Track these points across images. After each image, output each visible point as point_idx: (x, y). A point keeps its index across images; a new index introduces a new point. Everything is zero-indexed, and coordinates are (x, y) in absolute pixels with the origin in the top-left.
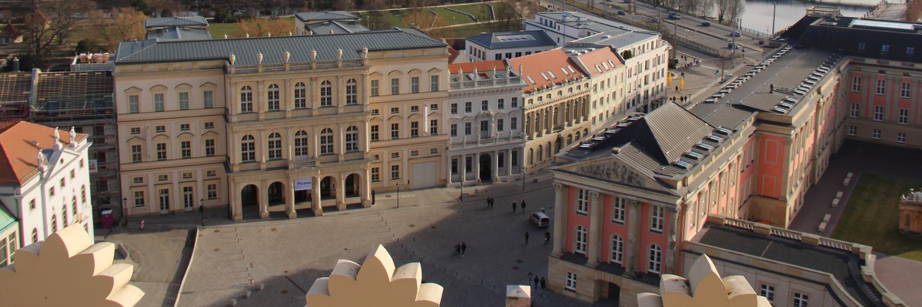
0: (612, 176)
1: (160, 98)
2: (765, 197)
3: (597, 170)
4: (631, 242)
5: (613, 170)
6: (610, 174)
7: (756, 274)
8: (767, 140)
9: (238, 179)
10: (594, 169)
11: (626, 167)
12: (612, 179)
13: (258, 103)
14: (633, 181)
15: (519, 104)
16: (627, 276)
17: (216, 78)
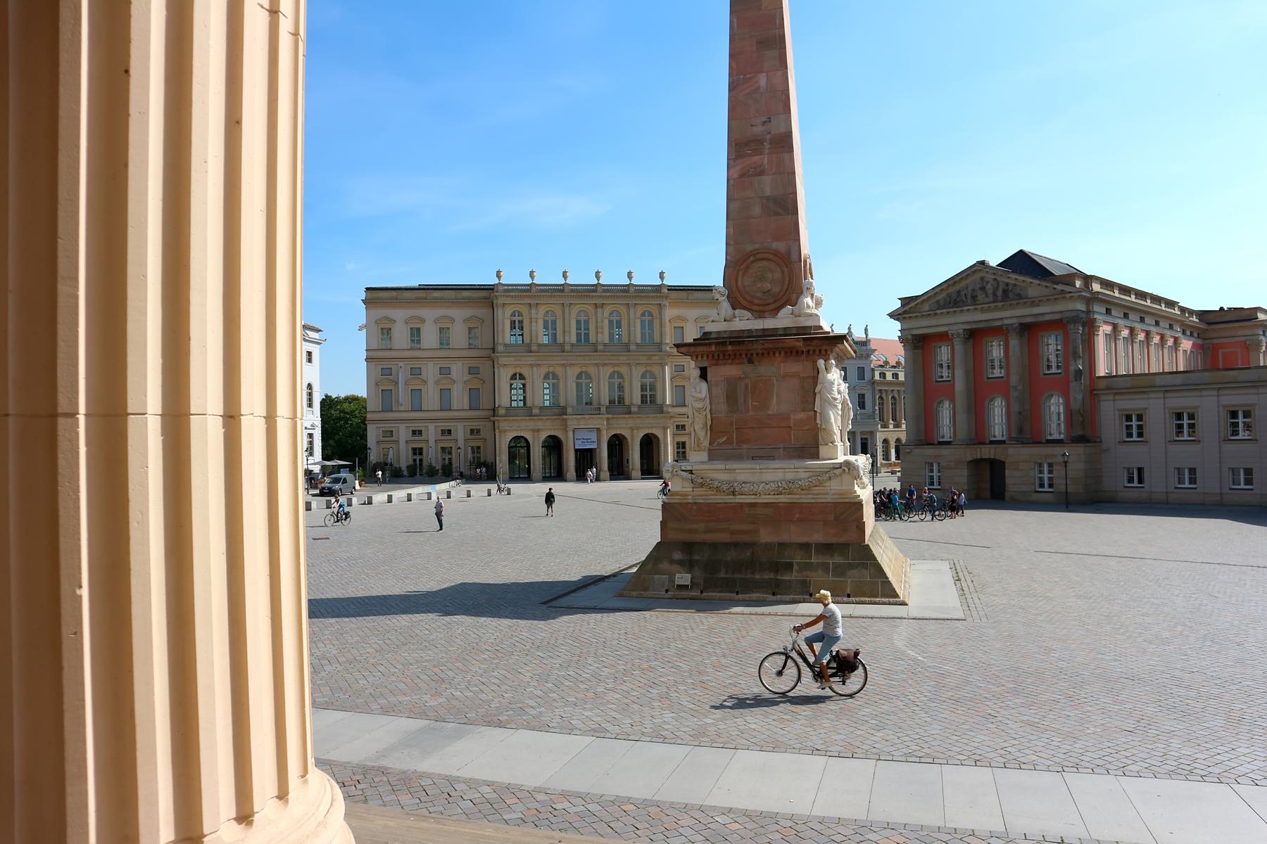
1: (416, 334)
4: (1015, 388)
6: (977, 296)
7: (1218, 396)
8: (1221, 352)
9: (503, 425)
13: (531, 331)
15: (867, 376)
17: (482, 312)
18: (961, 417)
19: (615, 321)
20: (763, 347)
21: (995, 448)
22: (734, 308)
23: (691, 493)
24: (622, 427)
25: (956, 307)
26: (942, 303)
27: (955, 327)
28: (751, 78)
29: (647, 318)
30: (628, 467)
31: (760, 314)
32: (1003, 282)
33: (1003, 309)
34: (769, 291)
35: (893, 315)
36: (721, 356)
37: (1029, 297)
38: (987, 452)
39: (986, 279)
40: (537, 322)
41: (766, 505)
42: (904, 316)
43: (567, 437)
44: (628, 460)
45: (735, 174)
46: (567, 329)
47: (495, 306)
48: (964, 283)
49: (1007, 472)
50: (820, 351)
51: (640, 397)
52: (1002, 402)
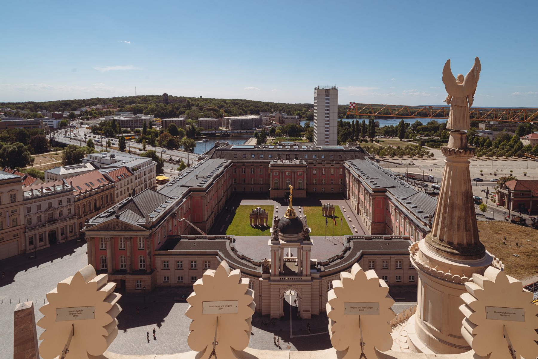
2: (197, 223)
5: (116, 225)
8: (195, 199)
10: (107, 226)
11: (123, 222)
12: (117, 229)
14: (127, 228)
35: (14, 281)
49: (126, 284)
51: (514, 225)
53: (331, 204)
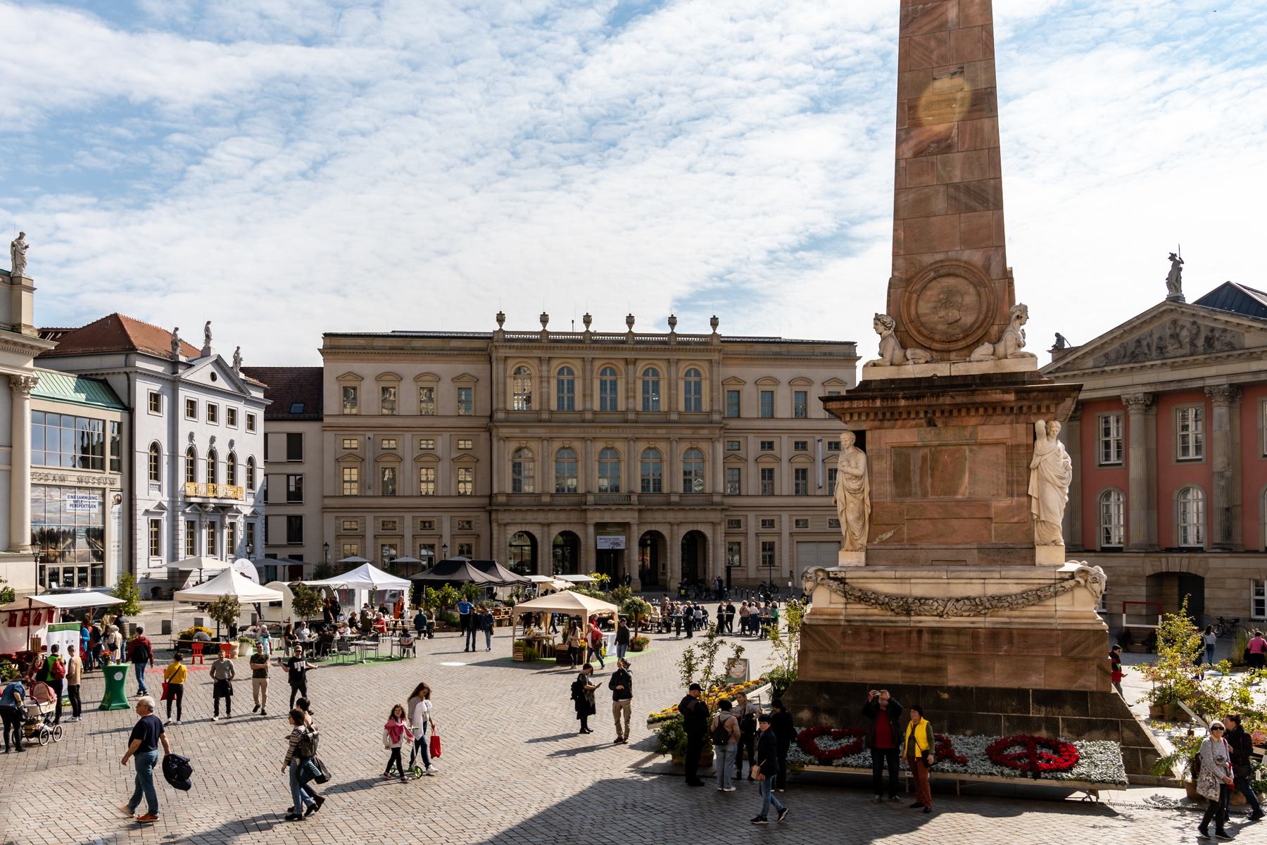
0: (1170, 348)
3: (1137, 347)
5: (1172, 336)
6: (1166, 347)
16: (1219, 550)
18: (1137, 513)
19: (651, 383)
20: (954, 401)
21: (1189, 557)
22: (904, 347)
23: (844, 612)
24: (660, 522)
25: (1135, 362)
26: (1113, 356)
27: (1131, 390)
28: (934, 8)
29: (693, 379)
30: (664, 574)
31: (942, 355)
32: (1206, 326)
33: (1205, 363)
34: (957, 321)
36: (888, 415)
37: (1246, 346)
38: (1176, 563)
39: (1180, 323)
40: (548, 382)
41: (959, 631)
42: (1057, 375)
43: (586, 534)
44: (664, 565)
45: (908, 153)
46: (588, 392)
47: (494, 358)
48: (1146, 329)
49: (1207, 593)
50: (1039, 408)
52: (1197, 493)
53: (46, 529)
